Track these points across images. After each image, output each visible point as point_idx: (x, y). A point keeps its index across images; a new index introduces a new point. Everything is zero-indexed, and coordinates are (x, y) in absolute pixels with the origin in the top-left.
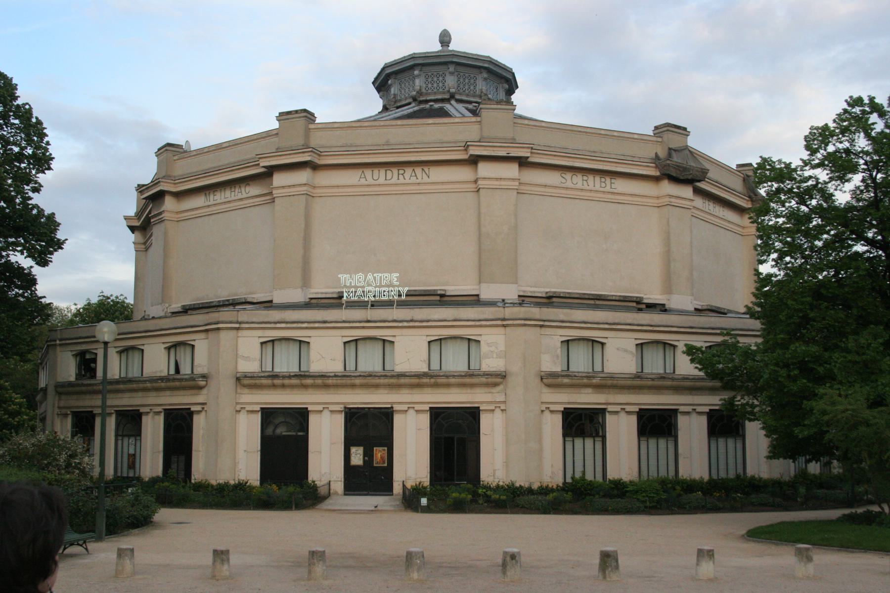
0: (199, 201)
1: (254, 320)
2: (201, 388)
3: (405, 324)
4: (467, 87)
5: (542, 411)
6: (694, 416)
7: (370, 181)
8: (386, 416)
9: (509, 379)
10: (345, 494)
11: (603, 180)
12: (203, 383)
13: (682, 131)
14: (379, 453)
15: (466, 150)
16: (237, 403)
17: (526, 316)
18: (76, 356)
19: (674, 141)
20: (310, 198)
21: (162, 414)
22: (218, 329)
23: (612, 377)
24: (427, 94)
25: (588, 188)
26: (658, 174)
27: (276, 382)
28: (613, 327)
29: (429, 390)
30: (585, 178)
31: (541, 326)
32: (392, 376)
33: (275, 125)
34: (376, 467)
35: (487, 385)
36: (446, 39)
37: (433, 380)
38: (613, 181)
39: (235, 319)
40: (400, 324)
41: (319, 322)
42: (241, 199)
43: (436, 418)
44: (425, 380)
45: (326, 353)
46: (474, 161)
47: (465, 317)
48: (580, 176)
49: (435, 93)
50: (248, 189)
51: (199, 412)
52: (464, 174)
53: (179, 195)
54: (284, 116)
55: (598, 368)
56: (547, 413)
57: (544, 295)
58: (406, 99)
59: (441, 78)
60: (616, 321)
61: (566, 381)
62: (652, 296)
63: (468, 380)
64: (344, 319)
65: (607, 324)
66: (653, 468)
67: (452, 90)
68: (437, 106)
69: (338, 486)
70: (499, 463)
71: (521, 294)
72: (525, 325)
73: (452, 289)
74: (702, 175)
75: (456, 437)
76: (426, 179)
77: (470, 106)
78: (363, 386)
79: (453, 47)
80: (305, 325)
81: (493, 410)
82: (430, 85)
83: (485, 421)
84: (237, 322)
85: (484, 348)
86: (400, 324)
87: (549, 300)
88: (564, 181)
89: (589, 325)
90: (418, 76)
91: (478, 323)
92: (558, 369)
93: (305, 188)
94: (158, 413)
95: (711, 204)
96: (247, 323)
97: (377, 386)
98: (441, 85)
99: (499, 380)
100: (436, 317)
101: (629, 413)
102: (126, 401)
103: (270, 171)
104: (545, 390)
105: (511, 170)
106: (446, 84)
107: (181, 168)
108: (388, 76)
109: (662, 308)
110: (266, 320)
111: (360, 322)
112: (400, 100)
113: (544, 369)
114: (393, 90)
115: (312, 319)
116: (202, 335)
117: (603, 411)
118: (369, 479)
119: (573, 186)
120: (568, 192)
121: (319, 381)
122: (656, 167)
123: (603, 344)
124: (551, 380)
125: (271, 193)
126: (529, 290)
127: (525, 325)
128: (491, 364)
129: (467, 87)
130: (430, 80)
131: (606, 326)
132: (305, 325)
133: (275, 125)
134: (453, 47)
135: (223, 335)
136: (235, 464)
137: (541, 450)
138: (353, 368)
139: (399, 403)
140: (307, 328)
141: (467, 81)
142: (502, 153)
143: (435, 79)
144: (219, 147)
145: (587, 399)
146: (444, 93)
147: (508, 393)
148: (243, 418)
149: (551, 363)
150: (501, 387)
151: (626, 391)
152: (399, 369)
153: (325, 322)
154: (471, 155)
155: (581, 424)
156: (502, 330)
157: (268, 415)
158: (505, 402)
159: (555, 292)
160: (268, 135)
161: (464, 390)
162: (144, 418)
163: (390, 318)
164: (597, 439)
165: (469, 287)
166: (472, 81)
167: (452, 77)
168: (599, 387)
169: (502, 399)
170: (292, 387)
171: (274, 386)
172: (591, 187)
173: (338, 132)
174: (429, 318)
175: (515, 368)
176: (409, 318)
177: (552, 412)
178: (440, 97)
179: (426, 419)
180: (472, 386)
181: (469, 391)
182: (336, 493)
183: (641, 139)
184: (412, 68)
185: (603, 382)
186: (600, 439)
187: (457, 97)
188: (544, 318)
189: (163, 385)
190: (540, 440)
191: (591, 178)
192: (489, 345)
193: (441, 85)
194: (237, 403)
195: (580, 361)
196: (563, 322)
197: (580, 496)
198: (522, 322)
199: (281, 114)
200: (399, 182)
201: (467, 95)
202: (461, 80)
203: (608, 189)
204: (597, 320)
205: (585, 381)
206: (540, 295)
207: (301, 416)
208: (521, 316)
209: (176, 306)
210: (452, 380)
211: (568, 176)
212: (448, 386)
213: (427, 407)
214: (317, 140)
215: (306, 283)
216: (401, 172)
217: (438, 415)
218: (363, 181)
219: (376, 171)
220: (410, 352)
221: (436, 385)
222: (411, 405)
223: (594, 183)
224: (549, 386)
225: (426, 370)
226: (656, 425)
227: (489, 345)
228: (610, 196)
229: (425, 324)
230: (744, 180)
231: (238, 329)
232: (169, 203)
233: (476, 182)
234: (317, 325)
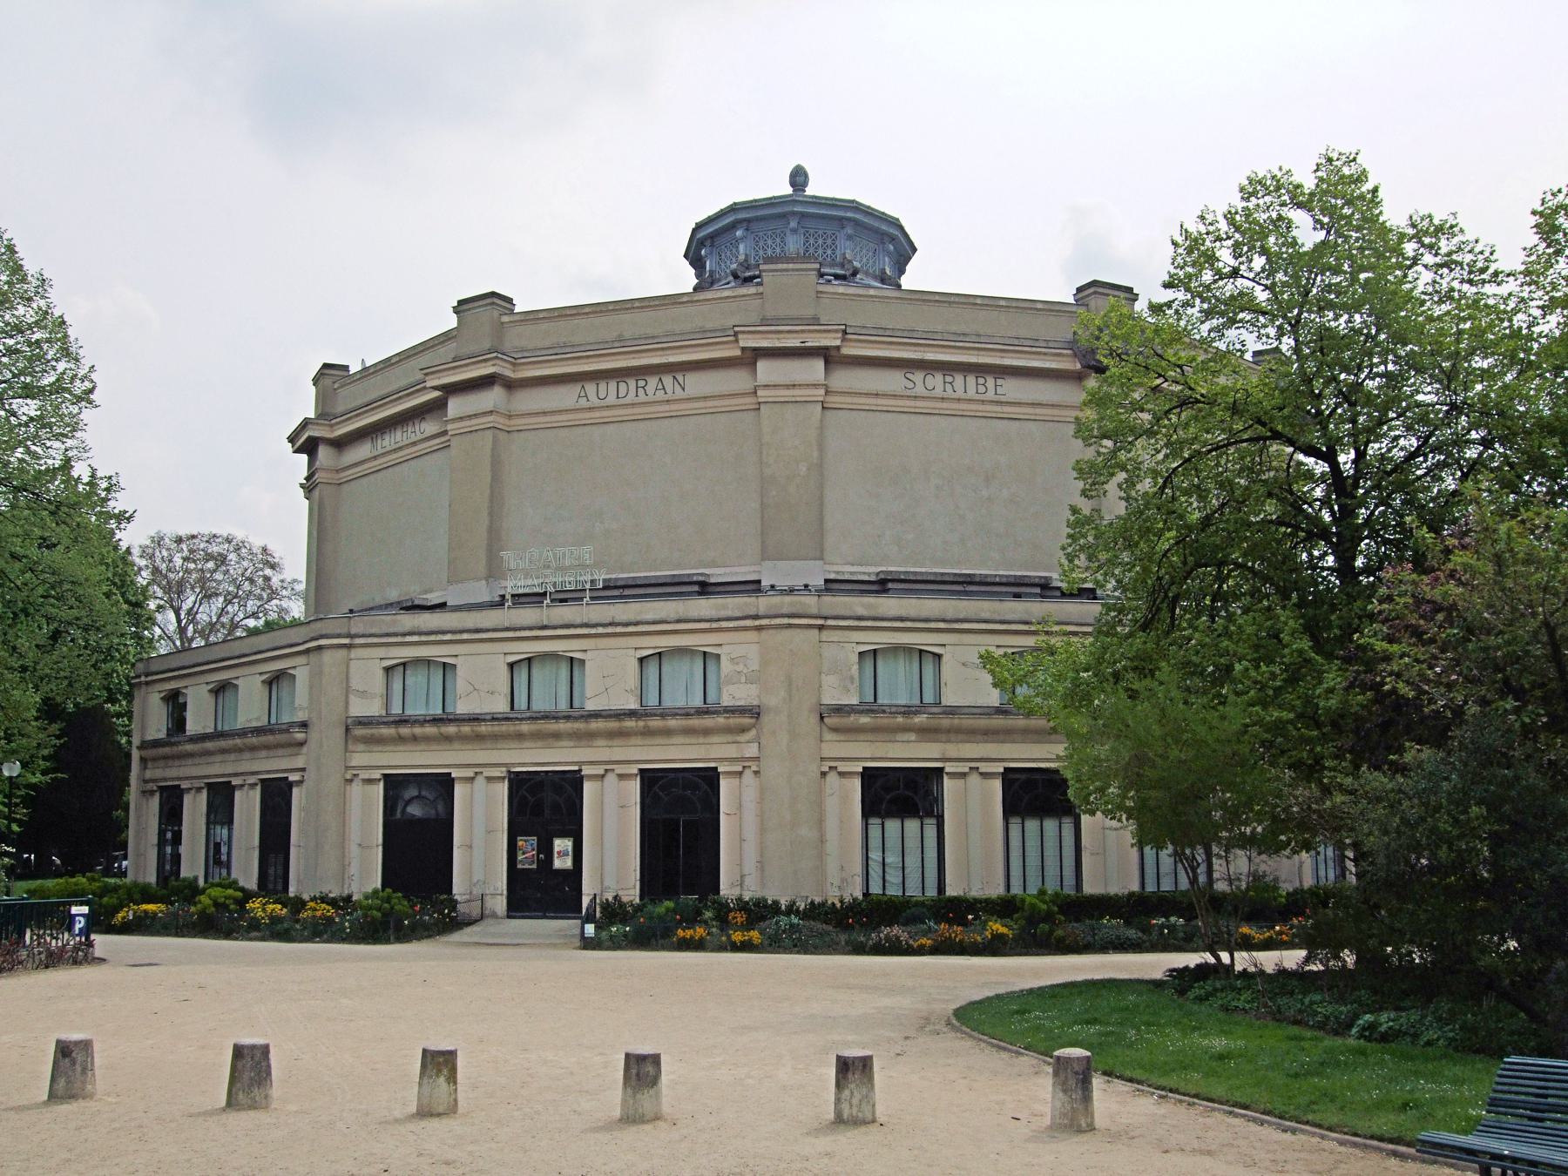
0: (363, 451)
1: (373, 631)
2: (301, 744)
3: (600, 630)
5: (824, 774)
6: (974, 779)
7: (594, 401)
9: (765, 719)
10: (509, 917)
11: (981, 381)
12: (300, 736)
14: (562, 844)
15: (737, 341)
16: (347, 768)
20: (502, 436)
21: (259, 788)
22: (320, 648)
25: (955, 396)
27: (405, 731)
28: (952, 626)
29: (639, 740)
30: (949, 379)
31: (821, 628)
33: (452, 322)
34: (558, 871)
35: (728, 730)
36: (800, 179)
37: (641, 724)
38: (999, 382)
39: (344, 631)
40: (593, 631)
41: (799, 626)
42: (414, 444)
43: (704, 778)
44: (630, 724)
45: (481, 683)
46: (753, 356)
47: (694, 614)
51: (300, 783)
52: (735, 380)
54: (462, 307)
55: (929, 698)
56: (832, 778)
57: (873, 578)
61: (865, 720)
64: (507, 624)
65: (944, 621)
66: (894, 877)
69: (500, 904)
71: (832, 576)
72: (790, 626)
73: (718, 575)
75: (680, 816)
76: (679, 393)
78: (537, 736)
79: (810, 190)
80: (448, 637)
81: (741, 773)
84: (349, 636)
85: (725, 662)
86: (593, 631)
89: (909, 624)
91: (714, 624)
93: (491, 418)
94: (253, 786)
96: (363, 636)
99: (747, 721)
100: (650, 617)
101: (985, 775)
102: (217, 769)
104: (828, 736)
107: (347, 398)
110: (391, 630)
111: (531, 629)
113: (827, 700)
115: (459, 626)
118: (541, 892)
119: (926, 393)
120: (919, 403)
121: (466, 729)
122: (1075, 355)
123: (938, 657)
126: (847, 571)
127: (790, 626)
128: (735, 694)
129: (820, 251)
131: (942, 625)
132: (448, 637)
133: (452, 322)
134: (810, 190)
135: (327, 656)
136: (343, 867)
138: (524, 706)
140: (451, 642)
142: (793, 342)
143: (769, 242)
144: (387, 363)
147: (763, 742)
148: (356, 789)
150: (753, 732)
153: (478, 631)
154: (743, 349)
155: (899, 795)
156: (752, 635)
157: (394, 785)
160: (446, 337)
162: (238, 794)
163: (578, 621)
164: (927, 821)
165: (743, 569)
168: (926, 733)
169: (752, 750)
170: (427, 739)
171: (401, 739)
172: (960, 393)
173: (544, 326)
174: (639, 618)
175: (772, 701)
176: (673, 616)
180: (706, 732)
182: (494, 915)
184: (733, 226)
185: (934, 722)
186: (934, 821)
190: (821, 822)
194: (347, 768)
195: (898, 684)
196: (860, 618)
197: (866, 924)
198: (786, 621)
199: (461, 302)
200: (637, 400)
203: (990, 395)
204: (924, 614)
205: (900, 719)
206: (866, 578)
207: (443, 785)
208: (785, 611)
210: (672, 723)
211: (918, 376)
213: (634, 769)
214: (515, 339)
215: (494, 571)
216: (641, 383)
218: (583, 403)
220: (611, 678)
221: (648, 733)
223: (965, 386)
226: (1032, 795)
231: (349, 647)
234: (465, 636)
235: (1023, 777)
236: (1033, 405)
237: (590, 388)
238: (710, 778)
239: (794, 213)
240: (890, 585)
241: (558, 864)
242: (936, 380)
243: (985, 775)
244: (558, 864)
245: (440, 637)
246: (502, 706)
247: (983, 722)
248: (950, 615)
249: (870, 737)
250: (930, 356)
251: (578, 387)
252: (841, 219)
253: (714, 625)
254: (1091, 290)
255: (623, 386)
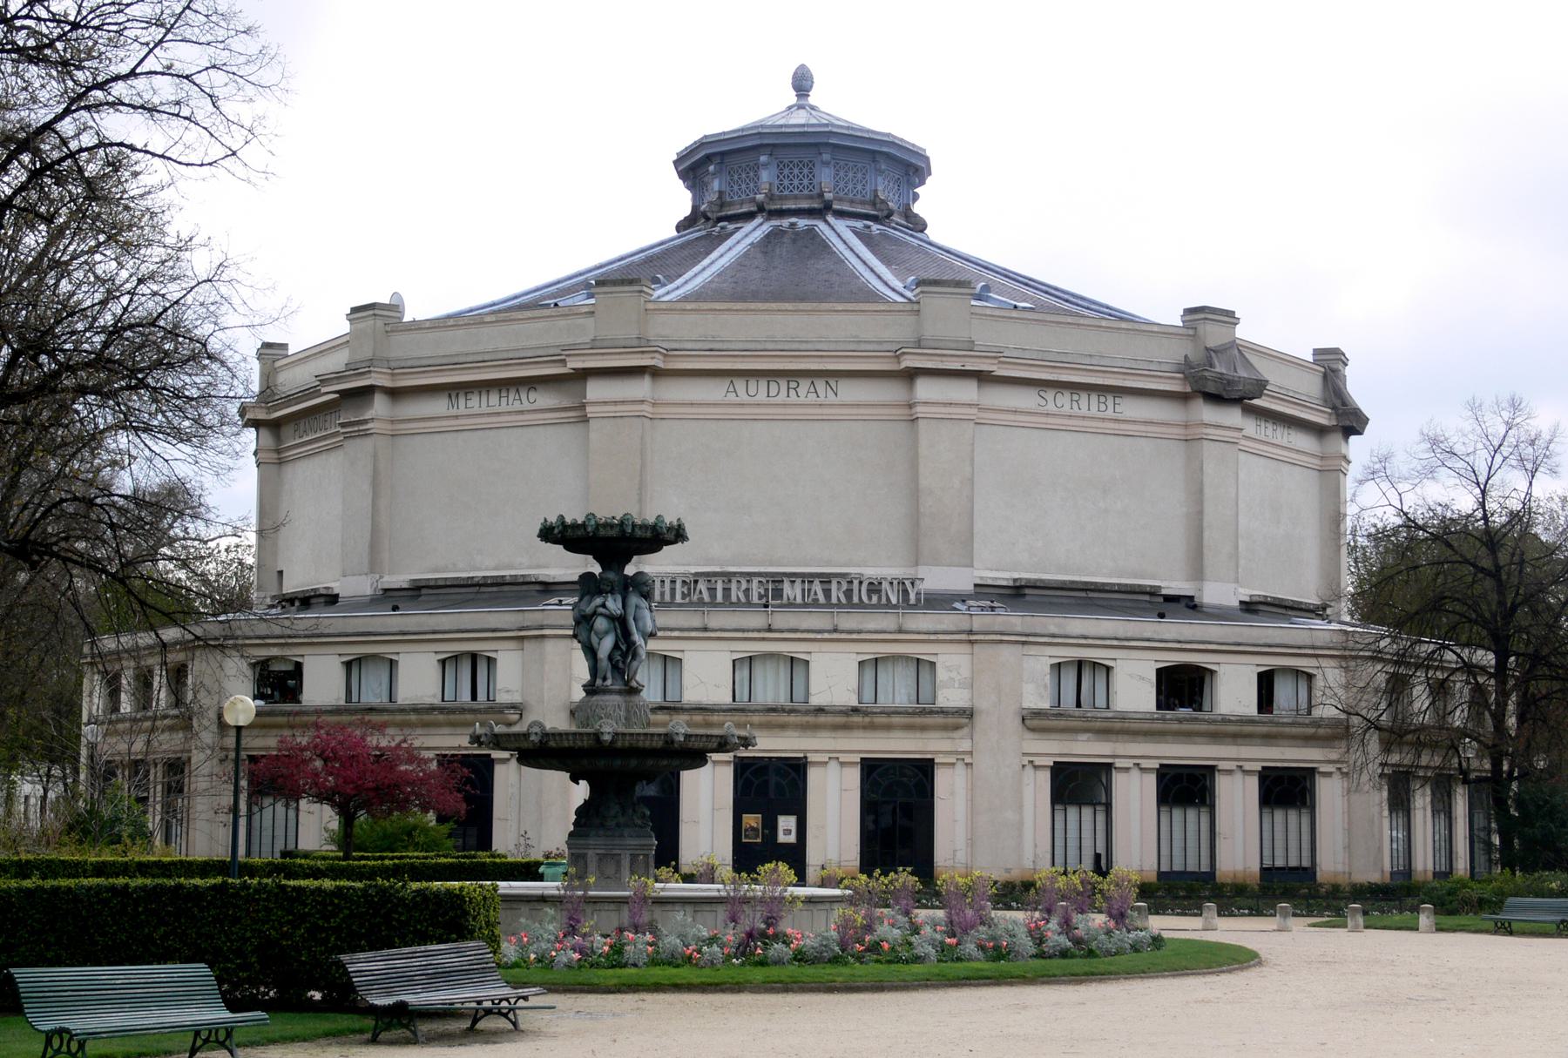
4: (850, 186)
6: (1239, 776)
7: (743, 397)
8: (794, 771)
9: (977, 718)
13: (1228, 317)
14: (787, 823)
17: (1002, 629)
18: (253, 666)
19: (1213, 335)
22: (543, 636)
23: (1123, 717)
24: (781, 198)
26: (1189, 390)
29: (860, 733)
30: (1075, 397)
31: (1024, 643)
32: (807, 712)
35: (945, 728)
37: (867, 719)
42: (521, 412)
43: (791, 766)
44: (857, 719)
46: (911, 375)
48: (1067, 394)
49: (796, 197)
50: (532, 395)
53: (395, 394)
56: (1029, 769)
58: (742, 203)
59: (806, 171)
60: (1129, 635)
62: (1173, 584)
63: (918, 720)
67: (828, 196)
68: (802, 223)
70: (961, 841)
74: (1260, 386)
77: (859, 224)
80: (676, 634)
82: (786, 182)
83: (942, 780)
85: (941, 674)
87: (1017, 594)
88: (1043, 402)
90: (765, 165)
91: (933, 637)
92: (1045, 704)
95: (1270, 426)
97: (783, 727)
98: (806, 182)
100: (872, 626)
101: (1143, 770)
103: (584, 375)
105: (967, 391)
106: (815, 182)
108: (708, 158)
109: (1187, 605)
112: (731, 204)
113: (1026, 705)
114: (716, 185)
116: (512, 645)
117: (1109, 766)
120: (1050, 420)
123: (1108, 669)
124: (1034, 721)
125: (583, 407)
128: (951, 697)
129: (850, 186)
130: (786, 171)
131: (1115, 643)
132: (676, 634)
135: (549, 645)
137: (1021, 823)
138: (746, 698)
139: (816, 751)
141: (851, 175)
145: (1085, 749)
146: (811, 197)
149: (1037, 697)
150: (966, 731)
151: (1140, 738)
152: (815, 701)
155: (1078, 786)
156: (966, 648)
158: (971, 753)
159: (1028, 580)
161: (911, 735)
166: (860, 175)
167: (826, 171)
169: (965, 745)
177: (1036, 767)
178: (805, 205)
179: (854, 776)
180: (924, 728)
181: (918, 735)
183: (1164, 332)
187: (836, 206)
188: (1028, 631)
189: (441, 717)
190: (1020, 807)
191: (1084, 396)
192: (949, 669)
193: (806, 182)
196: (1054, 636)
201: (852, 202)
202: (842, 174)
203: (1110, 413)
206: (1004, 583)
208: (996, 628)
209: (400, 579)
212: (888, 728)
213: (857, 758)
217: (872, 770)
218: (732, 397)
219: (752, 383)
220: (834, 677)
221: (872, 727)
222: (834, 756)
223: (1089, 405)
224: (1033, 730)
225: (855, 703)
227: (949, 669)
228: (1112, 425)
229: (854, 636)
230: (1325, 376)
232: (379, 407)
233: (911, 406)
234: (693, 634)
235: (1172, 772)
236: (1145, 423)
237: (740, 384)
238: (1211, 770)
239: (827, 144)
240: (1027, 591)
241: (782, 838)
242: (1064, 399)
243: (1143, 770)
244: (782, 838)
245: (669, 634)
246: (726, 699)
247: (1146, 726)
248: (1121, 634)
249: (1057, 736)
250: (1064, 378)
251: (727, 382)
252: (874, 152)
253: (932, 637)
254: (1196, 314)
255: (773, 386)
